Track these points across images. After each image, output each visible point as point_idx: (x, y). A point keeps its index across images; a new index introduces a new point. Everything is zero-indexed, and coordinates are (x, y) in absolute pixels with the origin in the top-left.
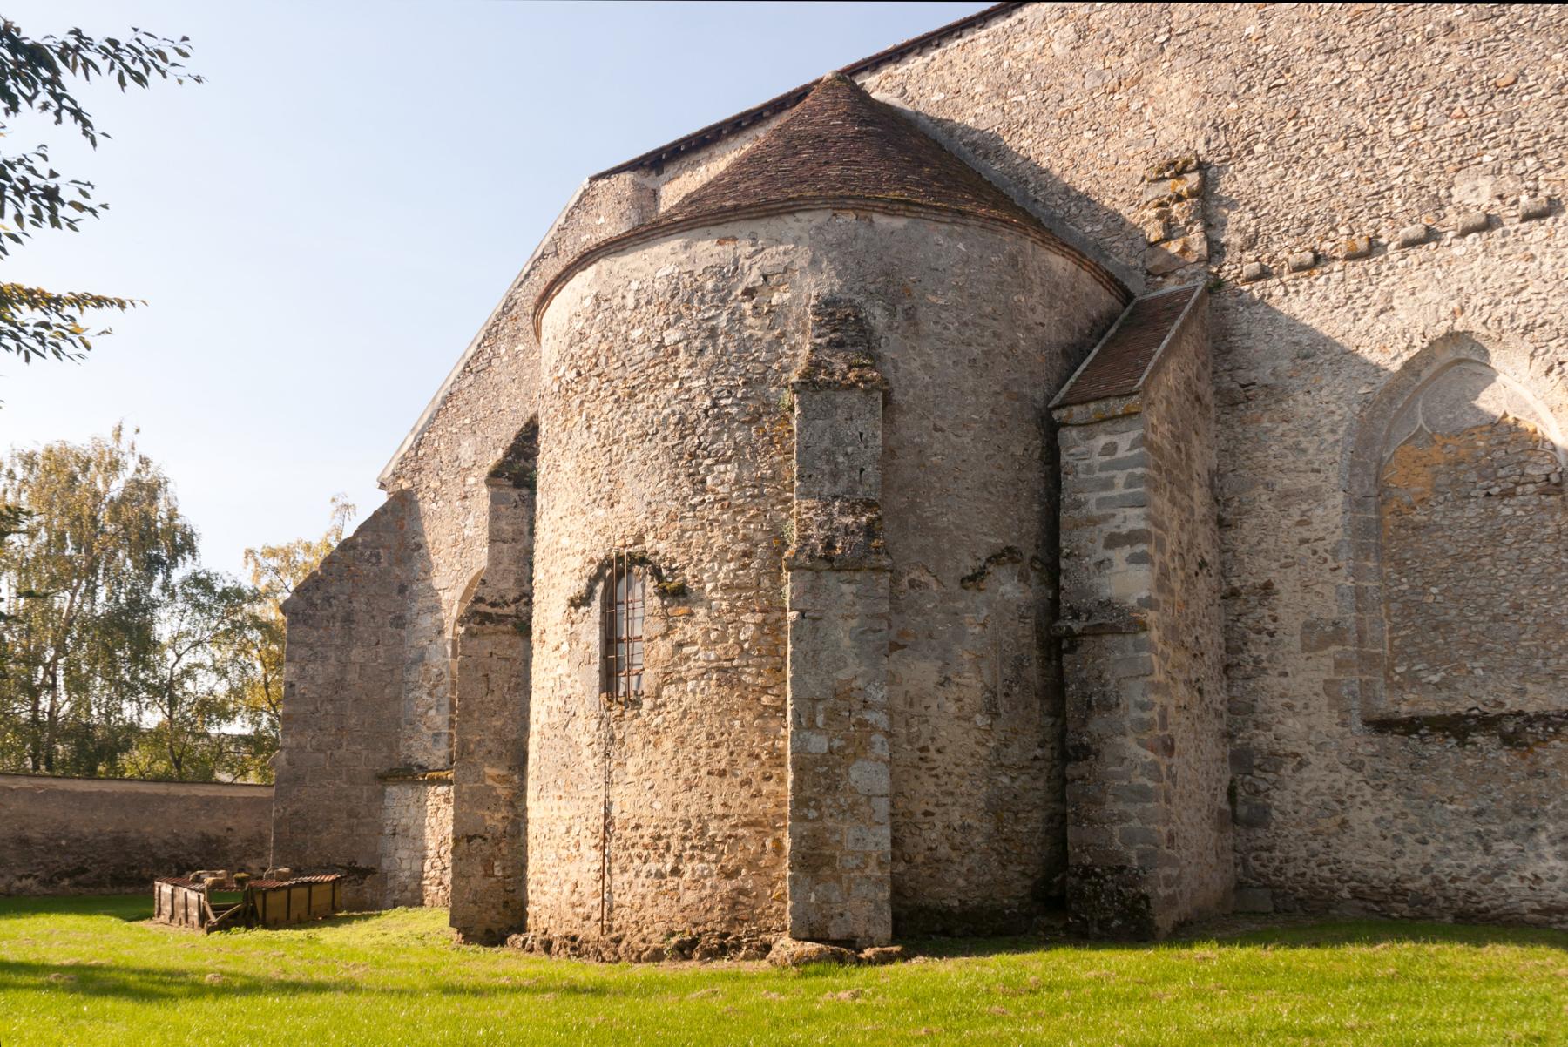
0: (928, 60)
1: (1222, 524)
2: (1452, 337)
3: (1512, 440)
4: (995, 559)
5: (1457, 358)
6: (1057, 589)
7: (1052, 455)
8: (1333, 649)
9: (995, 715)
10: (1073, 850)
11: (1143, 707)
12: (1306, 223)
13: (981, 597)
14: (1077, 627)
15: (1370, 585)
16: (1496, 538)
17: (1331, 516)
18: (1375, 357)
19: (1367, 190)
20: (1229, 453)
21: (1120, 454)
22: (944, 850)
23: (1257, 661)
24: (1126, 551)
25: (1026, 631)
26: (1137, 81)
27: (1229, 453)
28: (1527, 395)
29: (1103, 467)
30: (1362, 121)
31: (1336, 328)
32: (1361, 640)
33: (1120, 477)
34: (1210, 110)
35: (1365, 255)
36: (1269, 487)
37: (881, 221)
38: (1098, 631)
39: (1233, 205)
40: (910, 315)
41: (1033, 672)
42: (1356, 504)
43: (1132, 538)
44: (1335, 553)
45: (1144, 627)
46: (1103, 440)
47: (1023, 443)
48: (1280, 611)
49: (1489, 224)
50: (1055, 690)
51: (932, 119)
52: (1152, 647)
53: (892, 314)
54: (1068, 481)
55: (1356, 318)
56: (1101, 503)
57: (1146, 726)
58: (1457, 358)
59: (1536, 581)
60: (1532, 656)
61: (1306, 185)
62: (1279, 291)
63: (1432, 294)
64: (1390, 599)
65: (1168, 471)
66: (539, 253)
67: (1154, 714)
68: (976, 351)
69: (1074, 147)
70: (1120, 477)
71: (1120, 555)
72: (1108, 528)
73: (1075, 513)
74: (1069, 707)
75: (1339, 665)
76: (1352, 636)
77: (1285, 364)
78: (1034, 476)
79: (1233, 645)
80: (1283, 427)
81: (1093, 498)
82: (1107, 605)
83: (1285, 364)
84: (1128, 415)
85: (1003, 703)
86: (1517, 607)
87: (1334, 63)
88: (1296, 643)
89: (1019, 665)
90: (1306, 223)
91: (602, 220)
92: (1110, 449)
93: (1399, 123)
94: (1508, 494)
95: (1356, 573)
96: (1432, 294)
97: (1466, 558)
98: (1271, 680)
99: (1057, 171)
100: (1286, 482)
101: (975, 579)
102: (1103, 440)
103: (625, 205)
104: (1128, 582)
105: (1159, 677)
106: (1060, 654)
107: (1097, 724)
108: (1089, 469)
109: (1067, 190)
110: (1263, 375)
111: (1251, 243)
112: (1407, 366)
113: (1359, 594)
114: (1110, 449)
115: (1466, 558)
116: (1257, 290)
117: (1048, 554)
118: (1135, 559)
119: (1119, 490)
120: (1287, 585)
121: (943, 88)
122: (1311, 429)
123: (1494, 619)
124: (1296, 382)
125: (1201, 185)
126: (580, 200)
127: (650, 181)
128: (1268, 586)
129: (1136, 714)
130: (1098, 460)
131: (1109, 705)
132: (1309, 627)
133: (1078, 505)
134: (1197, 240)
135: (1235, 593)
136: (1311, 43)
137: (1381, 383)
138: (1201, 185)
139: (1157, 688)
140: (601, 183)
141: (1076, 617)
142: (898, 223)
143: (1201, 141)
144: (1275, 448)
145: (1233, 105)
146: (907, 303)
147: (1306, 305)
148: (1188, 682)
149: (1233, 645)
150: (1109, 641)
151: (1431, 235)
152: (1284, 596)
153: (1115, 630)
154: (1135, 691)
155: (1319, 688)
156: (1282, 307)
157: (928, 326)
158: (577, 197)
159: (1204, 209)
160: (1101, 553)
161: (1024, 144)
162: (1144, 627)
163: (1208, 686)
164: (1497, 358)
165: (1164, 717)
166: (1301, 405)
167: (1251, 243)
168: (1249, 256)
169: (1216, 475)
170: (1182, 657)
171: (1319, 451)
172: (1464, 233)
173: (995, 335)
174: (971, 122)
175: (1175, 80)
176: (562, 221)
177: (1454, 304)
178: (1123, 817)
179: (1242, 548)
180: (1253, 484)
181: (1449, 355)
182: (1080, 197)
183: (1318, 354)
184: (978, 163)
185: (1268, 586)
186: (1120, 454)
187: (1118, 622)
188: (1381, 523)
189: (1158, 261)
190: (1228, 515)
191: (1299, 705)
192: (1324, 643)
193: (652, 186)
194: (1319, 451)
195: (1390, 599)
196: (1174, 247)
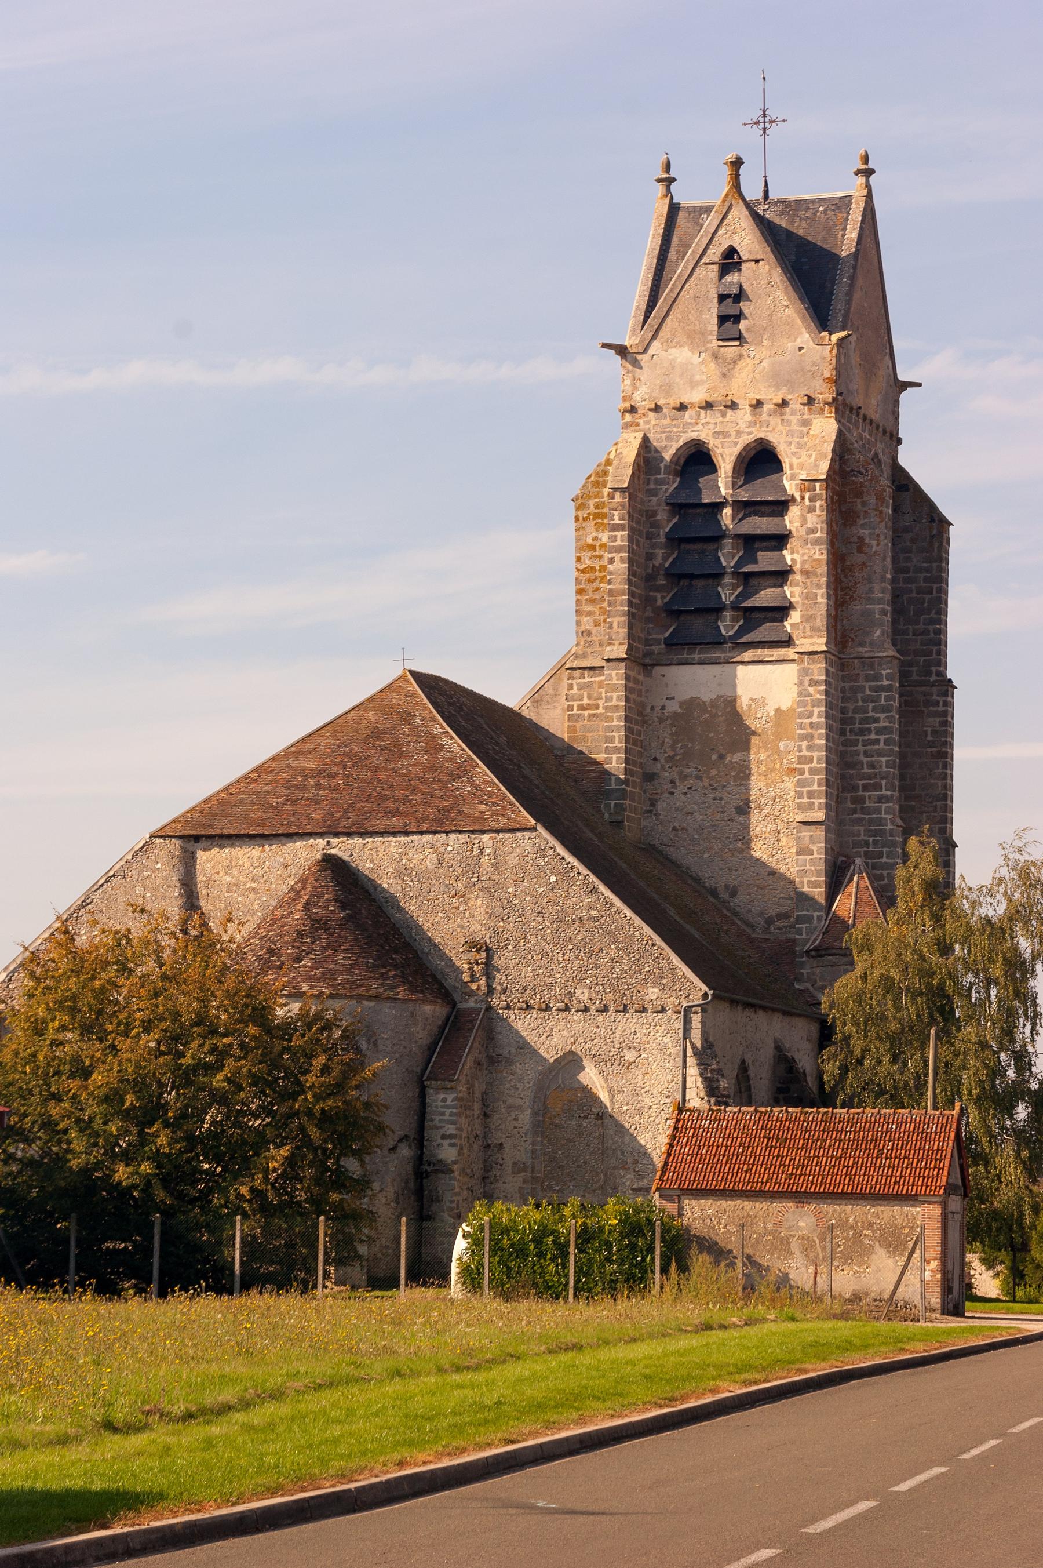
0: (364, 842)
1: (486, 1115)
2: (571, 1052)
3: (588, 1093)
4: (401, 1140)
5: (571, 1062)
6: (422, 1153)
7: (423, 1096)
8: (523, 1174)
9: (398, 1203)
10: (424, 1255)
11: (452, 1202)
12: (525, 988)
13: (395, 1156)
14: (429, 1169)
15: (538, 1148)
16: (580, 1135)
17: (526, 1118)
18: (545, 1055)
19: (548, 981)
20: (490, 1084)
21: (448, 1103)
22: (379, 1255)
23: (495, 1176)
24: (448, 1141)
25: (410, 1168)
26: (463, 896)
27: (490, 1084)
28: (595, 1080)
29: (442, 1107)
30: (548, 949)
31: (531, 1038)
32: (533, 1171)
33: (448, 1112)
34: (492, 923)
35: (546, 1010)
36: (504, 1102)
37: (365, 1003)
38: (437, 1171)
39: (498, 971)
40: (375, 1044)
41: (412, 1185)
42: (535, 1114)
43: (451, 1136)
44: (526, 1134)
45: (453, 1172)
46: (442, 1096)
47: (413, 1091)
48: (505, 1156)
49: (586, 1009)
50: (419, 1192)
51: (366, 876)
52: (455, 1179)
53: (369, 1043)
54: (428, 1109)
55: (540, 1037)
56: (440, 1121)
57: (451, 1209)
58: (571, 1062)
59: (591, 1154)
60: (588, 1183)
61: (527, 972)
62: (513, 1017)
63: (565, 1033)
64: (545, 1154)
65: (464, 1105)
66: (111, 873)
67: (454, 1205)
68: (398, 1055)
69: (434, 919)
70: (448, 1112)
71: (446, 1142)
72: (442, 1131)
73: (431, 1124)
74: (425, 1201)
75: (525, 1181)
76: (530, 1170)
77: (513, 1050)
78: (416, 1105)
79: (487, 1169)
80: (511, 1077)
81: (438, 1118)
82: (440, 1161)
83: (513, 1050)
84: (451, 1088)
85: (401, 1198)
86: (585, 1163)
87: (540, 919)
88: (509, 1170)
89: (406, 1183)
90: (525, 988)
91: (159, 866)
92: (445, 1100)
93: (560, 955)
94: (586, 1117)
95: (533, 1143)
96: (565, 1033)
97: (571, 1141)
98: (500, 1185)
99: (425, 928)
100: (510, 1101)
101: (393, 1149)
102: (442, 1096)
103: (175, 861)
104: (448, 1153)
105: (457, 1190)
106: (422, 1178)
107: (435, 1207)
108: (436, 1107)
109: (430, 939)
110: (505, 1052)
111: (504, 991)
112: (555, 1060)
113: (533, 1152)
114: (445, 1100)
115: (571, 1141)
116: (505, 1014)
117: (419, 1138)
118: (452, 1145)
119: (446, 1117)
120: (508, 1145)
121: (372, 861)
122: (521, 1080)
123: (578, 1166)
124: (517, 1059)
125: (486, 954)
126: (143, 847)
127: (190, 846)
128: (501, 1144)
129: (448, 1204)
130: (441, 1104)
131: (439, 1200)
132: (515, 1164)
133: (432, 1120)
134: (483, 982)
135: (489, 1146)
136: (533, 906)
137: (547, 1066)
138: (486, 954)
139: (457, 1194)
140: (158, 841)
141: (429, 1165)
142: (372, 1004)
143: (488, 936)
144: (508, 1086)
145: (501, 924)
146: (374, 1038)
147: (523, 1025)
148: (468, 1189)
149: (487, 1169)
150: (441, 1175)
151: (567, 1009)
152: (507, 1150)
153: (443, 1172)
154: (448, 1197)
155: (517, 1190)
156: (513, 1024)
157: (381, 1047)
158: (141, 845)
159: (487, 970)
160: (440, 1141)
161: (411, 907)
162: (453, 1172)
163: (475, 1188)
164: (585, 1062)
165: (458, 1205)
166: (518, 1068)
167: (504, 991)
168: (503, 997)
169: (484, 1094)
170: (466, 1179)
171: (523, 1090)
172: (578, 1011)
173: (405, 1047)
174: (385, 886)
175: (479, 902)
176: (130, 857)
177: (572, 1040)
178: (442, 1243)
179: (493, 1127)
180: (498, 1100)
181: (571, 1058)
182: (435, 944)
183: (524, 1046)
184: (390, 911)
185: (501, 1144)
186: (448, 1103)
187: (444, 1168)
188: (544, 1123)
189: (467, 990)
190: (488, 1112)
191: (509, 1196)
192: (519, 1172)
193: (191, 849)
194: (523, 1090)
195: (545, 1154)
196: (474, 987)
